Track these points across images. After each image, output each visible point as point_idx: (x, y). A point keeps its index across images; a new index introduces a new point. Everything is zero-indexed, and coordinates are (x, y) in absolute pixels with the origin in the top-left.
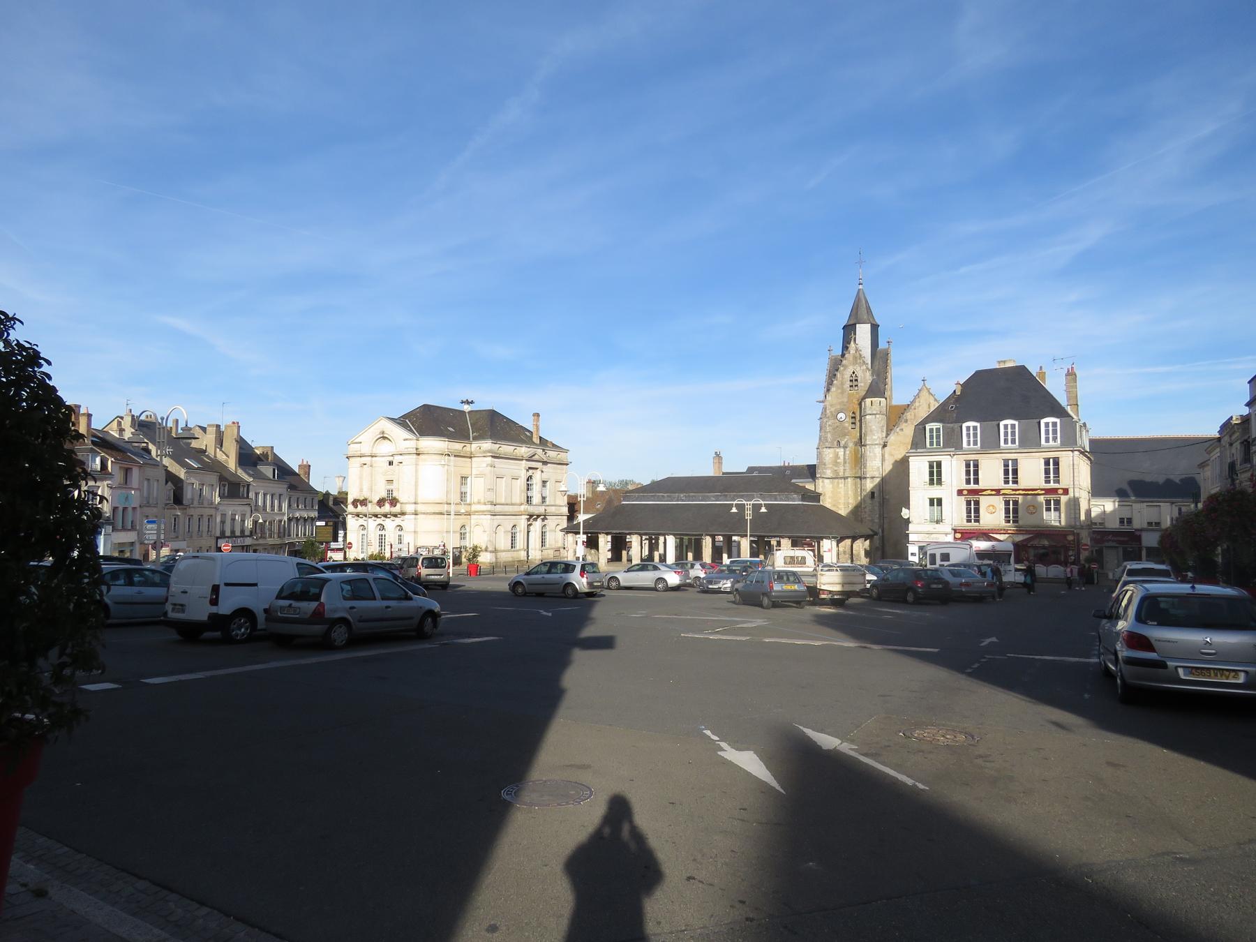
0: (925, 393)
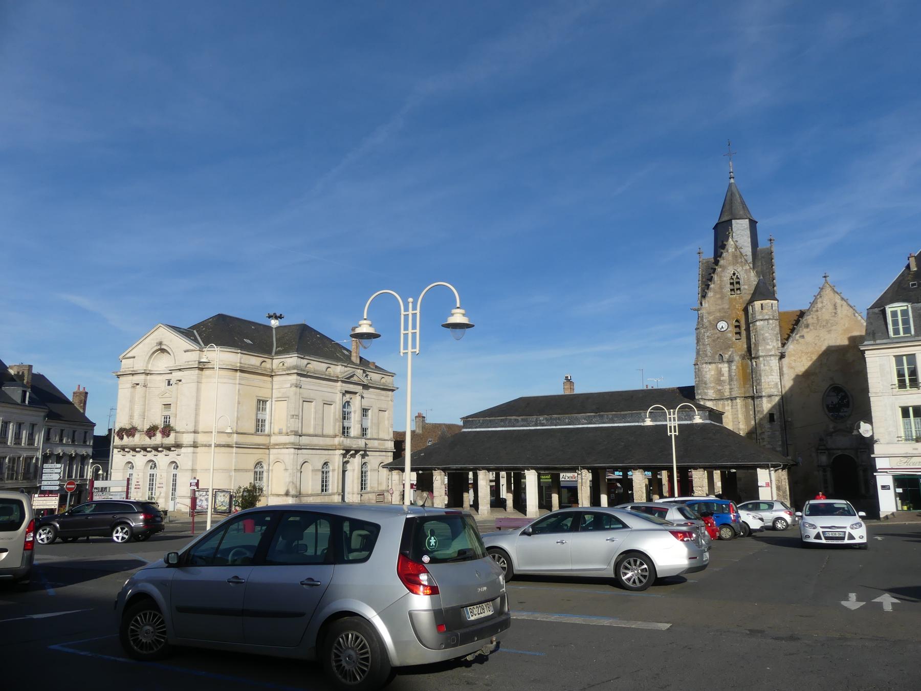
0: (828, 291)
